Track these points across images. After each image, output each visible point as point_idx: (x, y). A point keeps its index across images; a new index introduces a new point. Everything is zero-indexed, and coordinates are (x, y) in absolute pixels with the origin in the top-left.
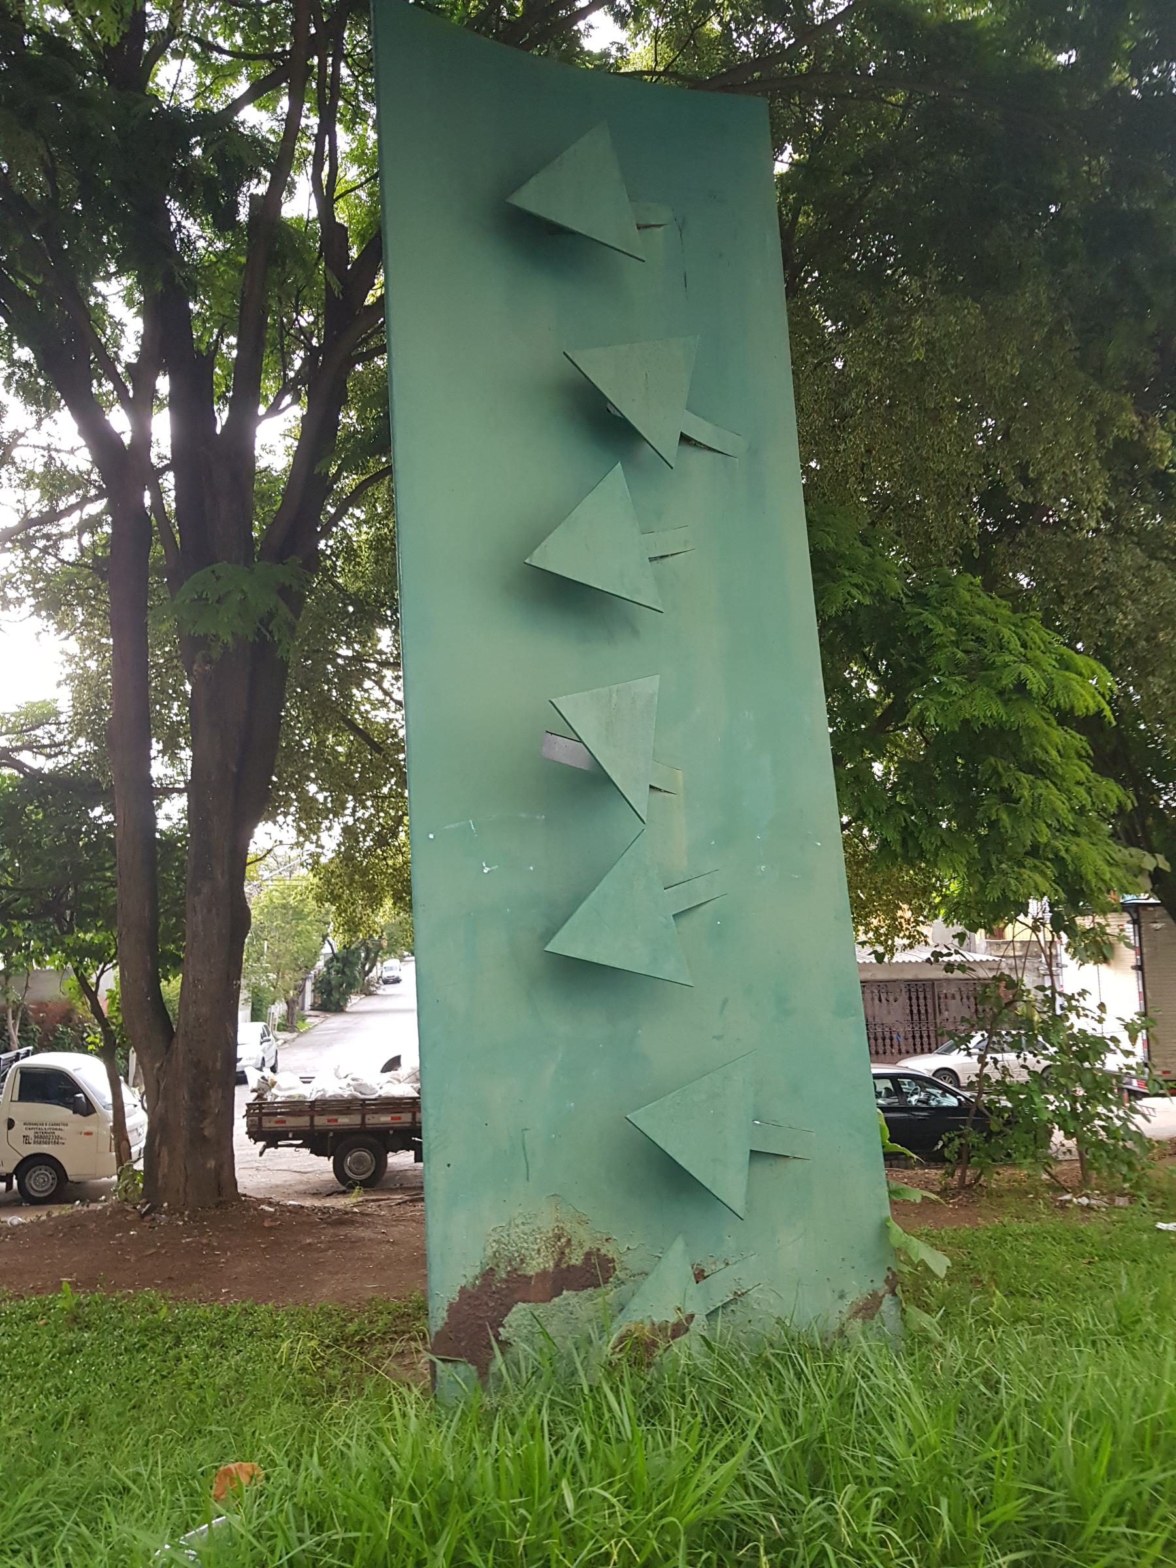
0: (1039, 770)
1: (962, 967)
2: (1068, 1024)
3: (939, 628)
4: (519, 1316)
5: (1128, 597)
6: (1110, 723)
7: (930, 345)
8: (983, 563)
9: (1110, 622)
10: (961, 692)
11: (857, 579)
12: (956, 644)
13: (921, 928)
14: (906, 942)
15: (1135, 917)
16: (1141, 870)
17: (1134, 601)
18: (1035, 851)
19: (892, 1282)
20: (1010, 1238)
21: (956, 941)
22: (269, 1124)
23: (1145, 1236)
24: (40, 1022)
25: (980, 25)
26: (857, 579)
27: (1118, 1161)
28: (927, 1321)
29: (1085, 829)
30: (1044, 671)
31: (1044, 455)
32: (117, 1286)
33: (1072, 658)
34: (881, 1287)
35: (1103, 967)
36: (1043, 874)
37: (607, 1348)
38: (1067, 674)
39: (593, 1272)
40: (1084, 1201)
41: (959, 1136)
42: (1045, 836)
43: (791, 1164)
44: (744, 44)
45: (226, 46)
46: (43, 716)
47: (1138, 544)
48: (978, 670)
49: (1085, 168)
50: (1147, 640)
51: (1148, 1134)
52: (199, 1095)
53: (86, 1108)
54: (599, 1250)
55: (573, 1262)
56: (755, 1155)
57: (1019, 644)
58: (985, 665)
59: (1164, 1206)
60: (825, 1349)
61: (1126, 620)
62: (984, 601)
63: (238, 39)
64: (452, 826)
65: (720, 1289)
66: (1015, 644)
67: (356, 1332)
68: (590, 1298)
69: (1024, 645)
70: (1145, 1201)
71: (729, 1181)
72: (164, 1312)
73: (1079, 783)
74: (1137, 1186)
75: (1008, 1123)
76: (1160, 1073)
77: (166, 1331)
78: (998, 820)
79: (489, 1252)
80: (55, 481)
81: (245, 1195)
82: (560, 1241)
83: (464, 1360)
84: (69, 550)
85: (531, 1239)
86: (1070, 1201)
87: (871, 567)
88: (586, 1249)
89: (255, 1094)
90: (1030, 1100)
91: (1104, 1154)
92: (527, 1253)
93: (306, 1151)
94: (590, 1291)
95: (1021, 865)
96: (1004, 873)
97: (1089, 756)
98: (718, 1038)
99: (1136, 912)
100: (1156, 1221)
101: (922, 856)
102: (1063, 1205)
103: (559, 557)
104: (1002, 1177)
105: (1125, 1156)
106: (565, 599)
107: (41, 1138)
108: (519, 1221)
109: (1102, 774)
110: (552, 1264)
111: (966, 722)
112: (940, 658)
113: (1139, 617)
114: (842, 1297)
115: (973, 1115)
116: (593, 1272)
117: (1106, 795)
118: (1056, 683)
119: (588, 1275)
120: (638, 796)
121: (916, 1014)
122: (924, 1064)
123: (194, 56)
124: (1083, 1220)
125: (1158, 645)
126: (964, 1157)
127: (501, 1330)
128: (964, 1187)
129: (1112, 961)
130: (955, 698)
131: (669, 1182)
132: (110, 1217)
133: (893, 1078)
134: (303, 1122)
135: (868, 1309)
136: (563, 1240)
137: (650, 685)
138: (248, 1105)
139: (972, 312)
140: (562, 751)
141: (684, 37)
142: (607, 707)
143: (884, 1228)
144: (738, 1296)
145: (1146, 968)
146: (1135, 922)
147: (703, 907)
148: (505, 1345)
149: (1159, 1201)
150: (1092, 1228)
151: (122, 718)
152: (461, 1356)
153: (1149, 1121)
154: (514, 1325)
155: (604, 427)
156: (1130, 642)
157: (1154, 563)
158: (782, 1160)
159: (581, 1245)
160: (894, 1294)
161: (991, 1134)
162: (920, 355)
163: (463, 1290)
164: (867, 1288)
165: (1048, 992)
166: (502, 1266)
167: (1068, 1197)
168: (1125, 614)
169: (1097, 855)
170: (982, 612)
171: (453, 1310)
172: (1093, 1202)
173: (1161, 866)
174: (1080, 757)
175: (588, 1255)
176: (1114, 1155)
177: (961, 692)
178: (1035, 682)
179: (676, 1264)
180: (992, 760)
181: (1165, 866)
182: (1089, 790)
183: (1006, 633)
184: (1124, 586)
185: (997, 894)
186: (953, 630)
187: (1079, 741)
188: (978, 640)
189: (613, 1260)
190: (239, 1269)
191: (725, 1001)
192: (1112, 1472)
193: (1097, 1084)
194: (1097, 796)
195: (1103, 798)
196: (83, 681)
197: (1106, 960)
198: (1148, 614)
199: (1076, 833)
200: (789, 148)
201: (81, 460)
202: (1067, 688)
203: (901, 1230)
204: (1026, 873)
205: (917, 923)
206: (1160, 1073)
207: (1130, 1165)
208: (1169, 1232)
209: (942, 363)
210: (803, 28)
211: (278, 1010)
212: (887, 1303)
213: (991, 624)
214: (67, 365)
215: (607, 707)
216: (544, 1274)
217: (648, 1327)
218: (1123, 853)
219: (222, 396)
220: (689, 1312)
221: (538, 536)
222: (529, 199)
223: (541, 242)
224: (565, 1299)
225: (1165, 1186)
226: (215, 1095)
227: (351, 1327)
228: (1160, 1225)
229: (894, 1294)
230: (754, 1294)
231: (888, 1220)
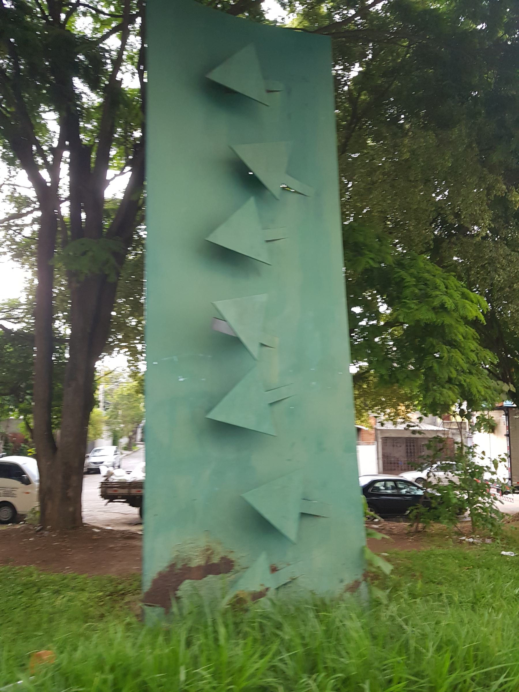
0: (453, 344)
1: (420, 432)
2: (467, 459)
3: (408, 279)
4: (186, 586)
5: (501, 268)
6: (483, 323)
7: (413, 152)
8: (437, 250)
9: (492, 279)
10: (416, 307)
11: (372, 256)
12: (415, 286)
13: (409, 415)
14: (402, 420)
15: (507, 412)
16: (502, 391)
17: (504, 270)
18: (450, 380)
19: (366, 575)
20: (433, 556)
21: (418, 421)
22: (110, 492)
23: (495, 558)
24: (13, 442)
25: (440, 11)
26: (372, 256)
27: (489, 523)
28: (381, 595)
29: (474, 371)
30: (454, 299)
31: (462, 202)
32: (19, 564)
33: (469, 294)
34: (360, 577)
35: (492, 434)
36: (453, 392)
37: (224, 603)
38: (465, 301)
39: (225, 566)
40: (471, 540)
41: (416, 509)
42: (454, 375)
43: (321, 520)
44: (337, 18)
45: (106, 11)
46: (14, 306)
47: (506, 244)
48: (424, 298)
49: (486, 76)
50: (510, 287)
51: (501, 510)
52: (67, 478)
53: (27, 482)
56: (303, 515)
57: (444, 286)
58: (427, 296)
59: (507, 544)
60: (321, 607)
61: (499, 278)
62: (430, 267)
63: (112, 9)
65: (283, 576)
66: (442, 287)
67: (121, 590)
68: (221, 579)
69: (447, 288)
70: (499, 541)
71: (289, 526)
72: (35, 576)
73: (472, 351)
74: (496, 534)
75: (439, 504)
76: (516, 483)
77: (35, 585)
78: (432, 367)
80: (22, 202)
81: (86, 524)
82: (208, 552)
84: (27, 232)
86: (464, 540)
87: (379, 251)
89: (105, 478)
90: (448, 494)
91: (480, 519)
93: (126, 505)
95: (443, 387)
96: (435, 391)
97: (477, 339)
99: (507, 411)
100: (502, 551)
101: (397, 382)
102: (461, 542)
103: (223, 238)
104: (435, 527)
105: (490, 520)
106: (227, 258)
107: (6, 495)
109: (485, 347)
111: (418, 321)
112: (407, 292)
113: (505, 277)
115: (426, 501)
116: (225, 566)
117: (485, 357)
118: (459, 304)
120: (253, 348)
121: (410, 453)
122: (410, 476)
123: (92, 15)
124: (469, 549)
125: (514, 290)
126: (417, 518)
128: (417, 532)
129: (496, 431)
131: (262, 527)
133: (395, 481)
134: (125, 491)
135: (354, 588)
137: (262, 298)
138: (102, 483)
139: (431, 138)
140: (222, 328)
141: (310, 13)
142: (238, 307)
143: (362, 552)
144: (293, 579)
145: (511, 435)
146: (506, 415)
148: (178, 598)
149: (505, 542)
150: (471, 552)
151: (43, 307)
152: (157, 604)
153: (503, 503)
155: (247, 181)
156: (501, 289)
157: (513, 253)
158: (317, 518)
161: (431, 508)
162: (407, 156)
164: (354, 578)
165: (460, 445)
167: (464, 538)
168: (499, 275)
169: (478, 384)
170: (428, 272)
172: (475, 541)
173: (511, 389)
174: (474, 339)
176: (486, 520)
177: (416, 307)
178: (449, 304)
179: (262, 563)
180: (431, 339)
181: (513, 390)
182: (477, 354)
183: (438, 281)
184: (499, 263)
185: (431, 400)
186: (414, 279)
187: (471, 331)
188: (426, 284)
190: (76, 558)
192: (451, 671)
193: (478, 488)
194: (481, 357)
195: (483, 358)
196: (29, 290)
197: (493, 431)
198: (510, 276)
199: (470, 373)
200: (357, 65)
201: (32, 194)
202: (464, 307)
204: (445, 391)
205: (408, 412)
206: (516, 483)
207: (493, 525)
208: (506, 556)
209: (417, 160)
210: (363, 11)
211: (124, 441)
212: (363, 587)
213: (432, 277)
214: (23, 151)
215: (238, 307)
216: (199, 567)
218: (493, 383)
219: (65, 162)
221: (212, 228)
222: (216, 76)
223: (222, 97)
225: (509, 534)
226: (74, 478)
227: (120, 587)
228: (503, 553)
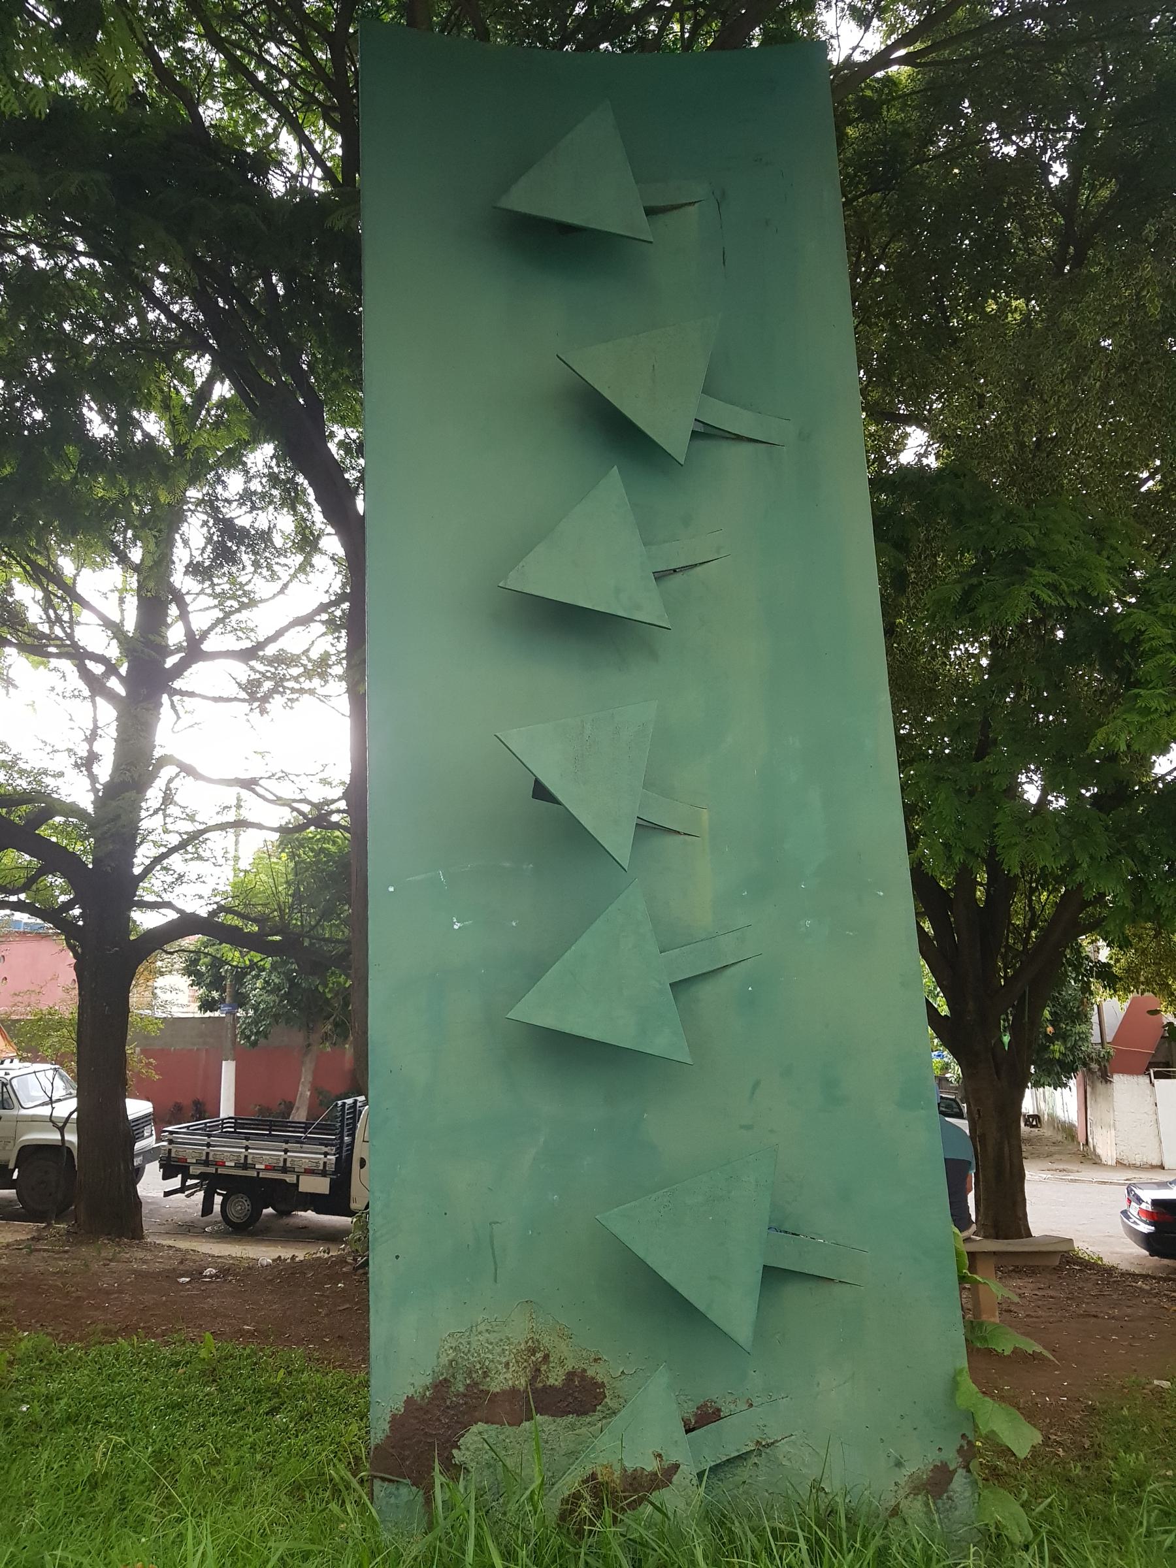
10: (1165, 707)
19: (967, 1453)
26: (1051, 577)
39: (579, 1397)
43: (837, 1289)
54: (584, 1370)
55: (551, 1382)
64: (418, 878)
65: (730, 1437)
68: (572, 1427)
71: (735, 1308)
79: (444, 1360)
82: (535, 1357)
83: (408, 1481)
88: (569, 1367)
92: (492, 1366)
94: (571, 1418)
98: (748, 1127)
106: (571, 626)
114: (899, 1464)
116: (579, 1397)
119: (570, 1399)
127: (455, 1452)
130: (1155, 716)
132: (330, 1267)
135: (936, 1483)
136: (538, 1355)
144: (762, 1447)
147: (733, 969)
154: (472, 1448)
155: (613, 432)
159: (562, 1363)
160: (969, 1471)
163: (409, 1401)
164: (934, 1458)
166: (459, 1377)
171: (396, 1422)
175: (571, 1375)
189: (603, 1385)
191: (757, 1084)
203: (976, 1389)
212: (959, 1483)
217: (617, 1474)
220: (673, 1460)
222: (523, 199)
223: (551, 245)
229: (969, 1471)
230: (784, 1447)
231: (962, 1370)
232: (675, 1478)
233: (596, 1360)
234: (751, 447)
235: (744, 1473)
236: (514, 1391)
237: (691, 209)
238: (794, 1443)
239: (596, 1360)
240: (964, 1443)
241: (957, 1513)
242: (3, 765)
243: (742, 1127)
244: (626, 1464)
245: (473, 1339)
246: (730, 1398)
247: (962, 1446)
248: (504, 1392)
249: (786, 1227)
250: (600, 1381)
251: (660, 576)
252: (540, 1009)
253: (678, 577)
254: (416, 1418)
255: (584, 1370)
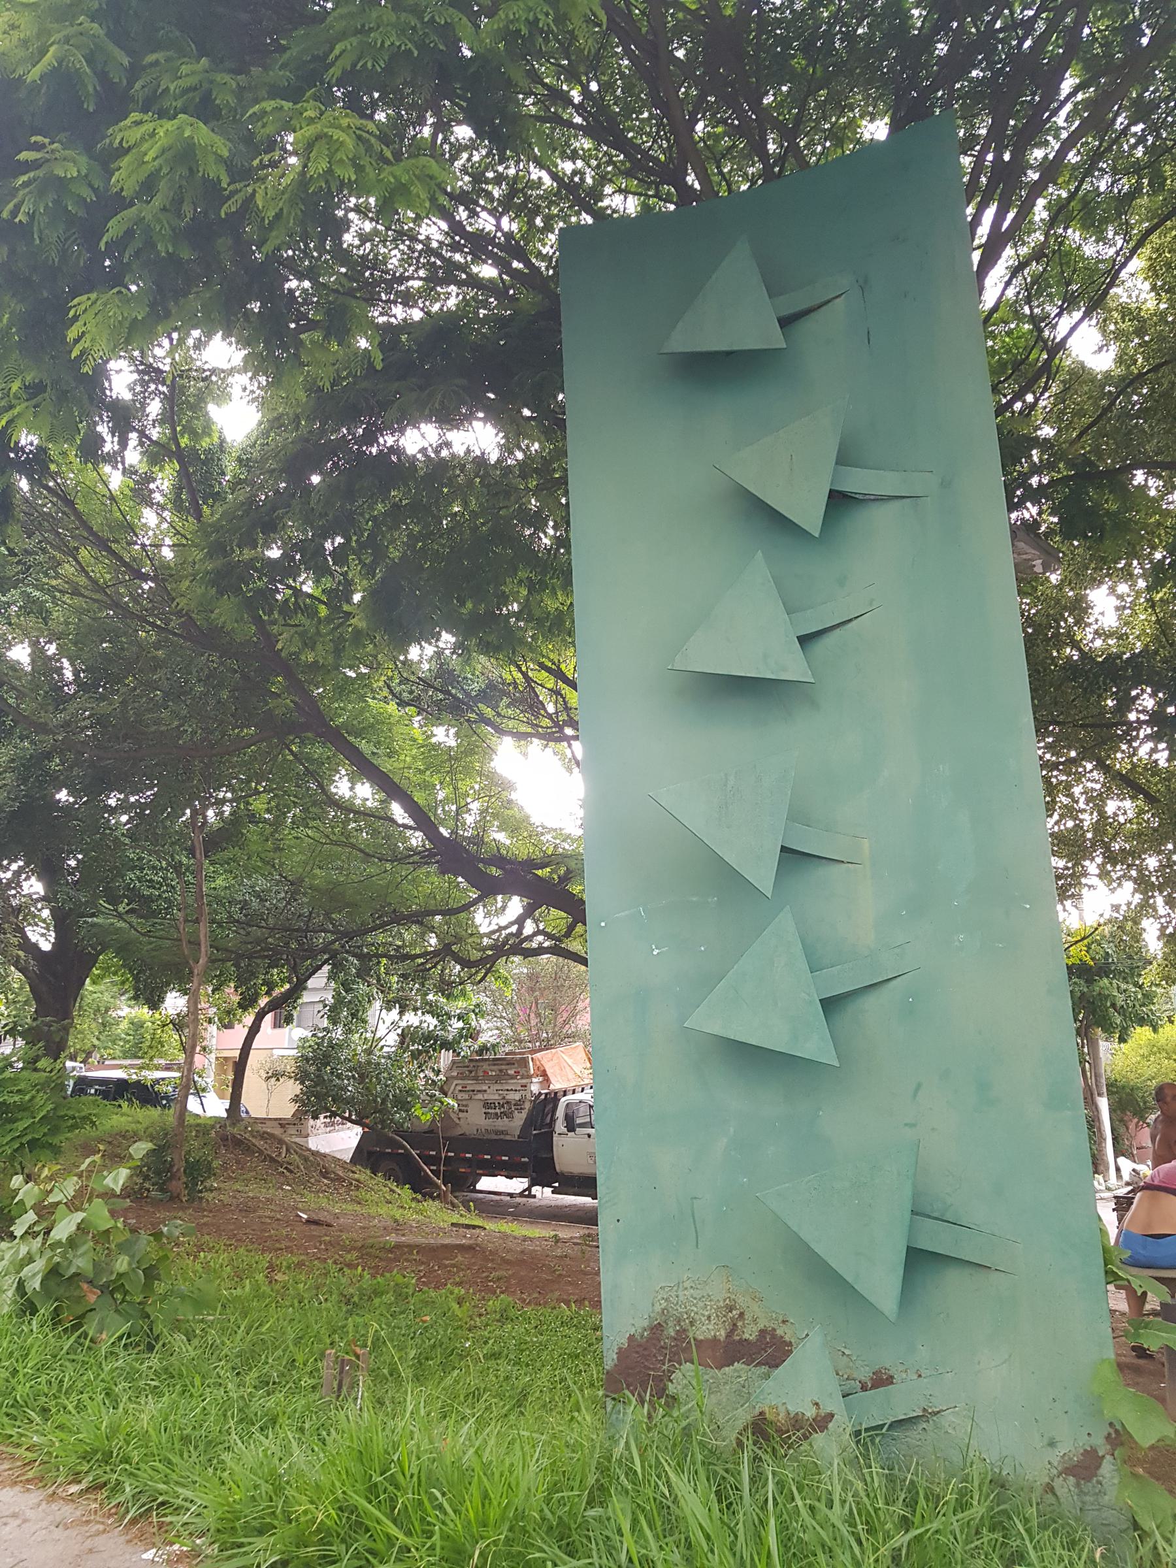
54: (774, 1330)
55: (746, 1336)
65: (898, 1402)
79: (658, 1308)
85: (701, 1304)
92: (697, 1317)
108: (687, 1284)
110: (723, 1333)
114: (1052, 1444)
135: (1084, 1468)
144: (927, 1415)
147: (894, 982)
159: (755, 1320)
163: (631, 1338)
164: (1084, 1443)
171: (620, 1352)
175: (763, 1332)
191: (919, 1086)
212: (1107, 1468)
222: (681, 341)
224: (735, 1370)
230: (948, 1418)
232: (830, 1425)
233: (784, 1322)
234: (908, 500)
235: (913, 1436)
236: (715, 1340)
237: (838, 300)
238: (957, 1413)
239: (784, 1322)
240: (1112, 1431)
241: (1106, 1498)
242: (1175, 209)
243: (906, 1125)
244: (790, 1408)
245: (680, 1293)
246: (901, 1368)
247: (1109, 1434)
248: (707, 1340)
249: (948, 1217)
250: (787, 1338)
251: (805, 640)
252: (713, 1020)
253: (837, 632)
254: (637, 1352)
255: (774, 1330)
